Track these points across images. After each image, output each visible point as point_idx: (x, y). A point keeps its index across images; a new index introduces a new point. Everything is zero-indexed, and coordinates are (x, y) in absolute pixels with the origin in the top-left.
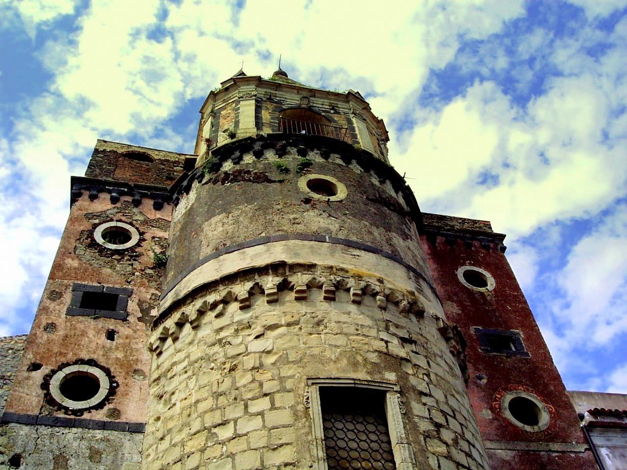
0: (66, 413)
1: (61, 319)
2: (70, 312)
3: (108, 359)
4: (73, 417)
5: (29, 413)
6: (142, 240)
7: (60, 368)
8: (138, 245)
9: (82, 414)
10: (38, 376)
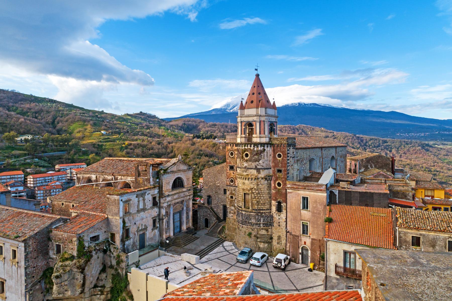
10: (228, 180)
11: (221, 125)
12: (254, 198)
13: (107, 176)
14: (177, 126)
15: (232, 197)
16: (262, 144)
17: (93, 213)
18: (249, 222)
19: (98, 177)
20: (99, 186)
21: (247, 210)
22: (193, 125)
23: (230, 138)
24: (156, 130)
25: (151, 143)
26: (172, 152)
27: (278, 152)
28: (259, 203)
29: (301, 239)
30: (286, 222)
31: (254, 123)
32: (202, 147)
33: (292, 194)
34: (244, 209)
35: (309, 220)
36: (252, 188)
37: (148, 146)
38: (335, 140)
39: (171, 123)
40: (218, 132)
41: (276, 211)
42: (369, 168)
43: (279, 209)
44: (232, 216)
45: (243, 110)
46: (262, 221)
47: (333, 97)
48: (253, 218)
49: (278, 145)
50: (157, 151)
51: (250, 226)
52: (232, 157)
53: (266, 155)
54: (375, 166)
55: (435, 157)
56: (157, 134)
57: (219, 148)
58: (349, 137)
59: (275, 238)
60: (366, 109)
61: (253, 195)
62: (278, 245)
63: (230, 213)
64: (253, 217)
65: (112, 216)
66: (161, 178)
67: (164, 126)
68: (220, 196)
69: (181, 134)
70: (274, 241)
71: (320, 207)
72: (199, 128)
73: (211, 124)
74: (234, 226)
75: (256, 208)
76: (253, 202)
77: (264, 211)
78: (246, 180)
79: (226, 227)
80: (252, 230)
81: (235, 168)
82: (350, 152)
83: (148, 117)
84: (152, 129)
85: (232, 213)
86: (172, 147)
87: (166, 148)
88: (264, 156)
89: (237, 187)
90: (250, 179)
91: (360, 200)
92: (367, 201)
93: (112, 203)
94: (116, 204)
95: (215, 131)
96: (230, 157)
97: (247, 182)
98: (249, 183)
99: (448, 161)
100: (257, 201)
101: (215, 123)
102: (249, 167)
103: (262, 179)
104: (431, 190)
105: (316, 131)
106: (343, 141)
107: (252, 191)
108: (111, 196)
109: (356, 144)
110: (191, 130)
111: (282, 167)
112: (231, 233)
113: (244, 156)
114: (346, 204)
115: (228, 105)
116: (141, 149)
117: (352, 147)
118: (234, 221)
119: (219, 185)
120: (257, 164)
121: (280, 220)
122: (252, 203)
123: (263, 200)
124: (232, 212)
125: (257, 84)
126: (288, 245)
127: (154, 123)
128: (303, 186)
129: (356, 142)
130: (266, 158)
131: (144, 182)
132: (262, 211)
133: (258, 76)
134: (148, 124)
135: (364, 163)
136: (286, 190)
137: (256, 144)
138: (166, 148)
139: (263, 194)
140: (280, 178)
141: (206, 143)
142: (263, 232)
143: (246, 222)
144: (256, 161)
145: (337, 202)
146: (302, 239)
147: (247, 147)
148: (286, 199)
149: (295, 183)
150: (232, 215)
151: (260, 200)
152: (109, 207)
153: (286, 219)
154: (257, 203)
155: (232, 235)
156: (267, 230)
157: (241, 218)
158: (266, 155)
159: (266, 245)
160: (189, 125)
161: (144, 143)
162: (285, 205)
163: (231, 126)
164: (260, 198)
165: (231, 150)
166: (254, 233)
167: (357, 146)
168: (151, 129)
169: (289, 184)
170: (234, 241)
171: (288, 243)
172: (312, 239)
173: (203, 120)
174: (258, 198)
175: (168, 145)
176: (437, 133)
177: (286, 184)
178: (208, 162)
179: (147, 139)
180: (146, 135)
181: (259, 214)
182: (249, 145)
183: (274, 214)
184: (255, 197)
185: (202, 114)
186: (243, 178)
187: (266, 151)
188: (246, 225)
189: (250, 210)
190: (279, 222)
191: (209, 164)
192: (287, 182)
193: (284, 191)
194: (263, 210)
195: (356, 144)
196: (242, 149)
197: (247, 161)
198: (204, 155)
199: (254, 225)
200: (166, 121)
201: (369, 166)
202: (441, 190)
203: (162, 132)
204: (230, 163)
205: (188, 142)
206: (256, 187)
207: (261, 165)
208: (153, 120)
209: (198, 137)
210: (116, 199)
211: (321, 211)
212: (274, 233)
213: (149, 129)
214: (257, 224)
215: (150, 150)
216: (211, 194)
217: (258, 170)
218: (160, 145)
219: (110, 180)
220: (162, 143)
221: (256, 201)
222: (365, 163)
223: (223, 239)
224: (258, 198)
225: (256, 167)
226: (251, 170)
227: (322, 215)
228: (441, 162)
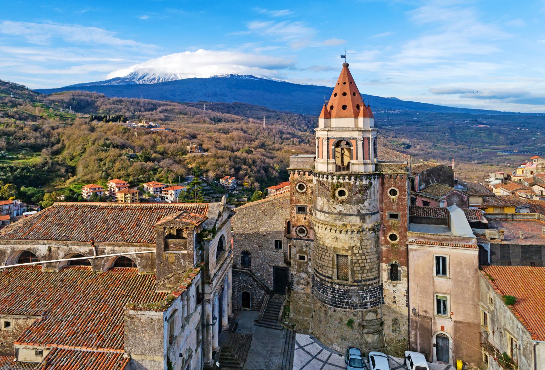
2: (297, 213)
6: (307, 188)
8: (306, 190)
10: (294, 229)
11: (129, 101)
12: (356, 263)
13: (76, 247)
14: (62, 102)
15: (302, 258)
16: (369, 176)
17: (84, 349)
19: (53, 249)
20: (55, 267)
21: (344, 282)
22: (87, 101)
23: (298, 162)
24: (28, 108)
25: (22, 129)
26: (58, 141)
27: (390, 187)
28: (364, 270)
29: (435, 323)
30: (408, 296)
31: (353, 142)
32: (106, 133)
33: (417, 252)
34: (337, 281)
35: (448, 292)
36: (353, 247)
37: (17, 134)
38: (279, 120)
39: (52, 98)
40: (125, 110)
41: (388, 279)
42: (431, 184)
43: (394, 276)
44: (303, 289)
45: (329, 120)
46: (368, 298)
47: (251, 66)
48: (354, 295)
49: (391, 175)
50: (33, 141)
51: (349, 308)
53: (372, 192)
54: (437, 180)
55: (385, 140)
56: (30, 115)
57: (133, 135)
58: (294, 117)
59: (388, 322)
60: (309, 83)
61: (354, 258)
62: (394, 334)
63: (298, 283)
64: (355, 293)
65: (143, 354)
66: (205, 247)
67: (41, 101)
68: (268, 252)
69: (71, 114)
70: (385, 327)
71: (468, 272)
72: (96, 104)
73: (114, 100)
74: (308, 306)
75: (360, 279)
76: (355, 269)
77: (371, 282)
78: (341, 233)
79: (291, 307)
80: (354, 315)
81: (308, 210)
82: (297, 136)
83: (12, 88)
84: (22, 107)
85: (303, 284)
86: (59, 135)
87: (49, 135)
88: (370, 193)
89: (312, 241)
90: (349, 233)
91: (522, 256)
92: (532, 258)
93: (142, 327)
94: (153, 329)
95: (121, 109)
96: (297, 191)
97: (343, 236)
98: (347, 238)
99: (397, 143)
100: (361, 267)
101: (121, 98)
102: (347, 213)
103: (369, 230)
104: (501, 207)
105: (256, 110)
106: (288, 122)
107: (352, 252)
108: (139, 312)
109: (303, 126)
110: (84, 107)
111: (398, 209)
112: (301, 318)
113: (337, 195)
114: (502, 264)
115: (135, 74)
116: (5, 138)
117: (299, 130)
118: (308, 298)
120: (361, 208)
121: (396, 294)
123: (370, 264)
124: (302, 281)
125: (349, 80)
126: (413, 333)
127: (23, 98)
128: (438, 239)
129: (302, 123)
130: (372, 196)
131: (179, 260)
132: (368, 283)
133: (346, 66)
134: (13, 99)
135: (424, 177)
136: (407, 245)
137: (358, 176)
138: (49, 135)
139: (369, 254)
140: (394, 226)
141: (112, 128)
142: (371, 316)
143: (341, 302)
144: (359, 202)
145: (489, 261)
146: (437, 321)
147: (344, 179)
148: (408, 260)
149: (423, 235)
150: (303, 287)
151: (366, 265)
152: (133, 336)
153: (408, 291)
154: (361, 269)
155: (303, 320)
156: (376, 312)
157: (329, 296)
158: (372, 192)
159: (376, 336)
160: (81, 100)
161: (10, 129)
162: (406, 269)
163: (144, 103)
164: (365, 261)
165: (300, 180)
166: (357, 320)
167: (305, 128)
168: (19, 107)
169: (412, 237)
170: (310, 331)
171: (412, 329)
172: (455, 321)
173: (102, 94)
174: (362, 262)
175: (52, 131)
176: (383, 112)
177: (406, 236)
178: (120, 155)
179: (15, 123)
180: (13, 117)
181: (365, 288)
182: (347, 177)
183: (384, 283)
184: (358, 260)
185: (96, 85)
186: (336, 231)
187: (372, 186)
188: (342, 308)
189: (349, 282)
190: (394, 297)
191: (122, 160)
192: (408, 234)
193: (403, 248)
194: (369, 280)
195: (303, 126)
196: (333, 183)
197: (342, 202)
198: (111, 145)
199: (356, 306)
200: (43, 95)
201: (430, 181)
202: (512, 207)
203: (40, 111)
204: (298, 201)
205: (84, 126)
207: (367, 208)
208: (21, 92)
209: (100, 119)
210: (154, 318)
211: (469, 278)
212: (384, 315)
213: (16, 107)
214: (361, 305)
215: (20, 140)
216: (249, 248)
217: (363, 217)
218: (38, 132)
219: (84, 253)
220: (40, 128)
221: (359, 266)
222: (426, 177)
225: (359, 211)
226: (351, 218)
227: (471, 284)
228: (391, 144)
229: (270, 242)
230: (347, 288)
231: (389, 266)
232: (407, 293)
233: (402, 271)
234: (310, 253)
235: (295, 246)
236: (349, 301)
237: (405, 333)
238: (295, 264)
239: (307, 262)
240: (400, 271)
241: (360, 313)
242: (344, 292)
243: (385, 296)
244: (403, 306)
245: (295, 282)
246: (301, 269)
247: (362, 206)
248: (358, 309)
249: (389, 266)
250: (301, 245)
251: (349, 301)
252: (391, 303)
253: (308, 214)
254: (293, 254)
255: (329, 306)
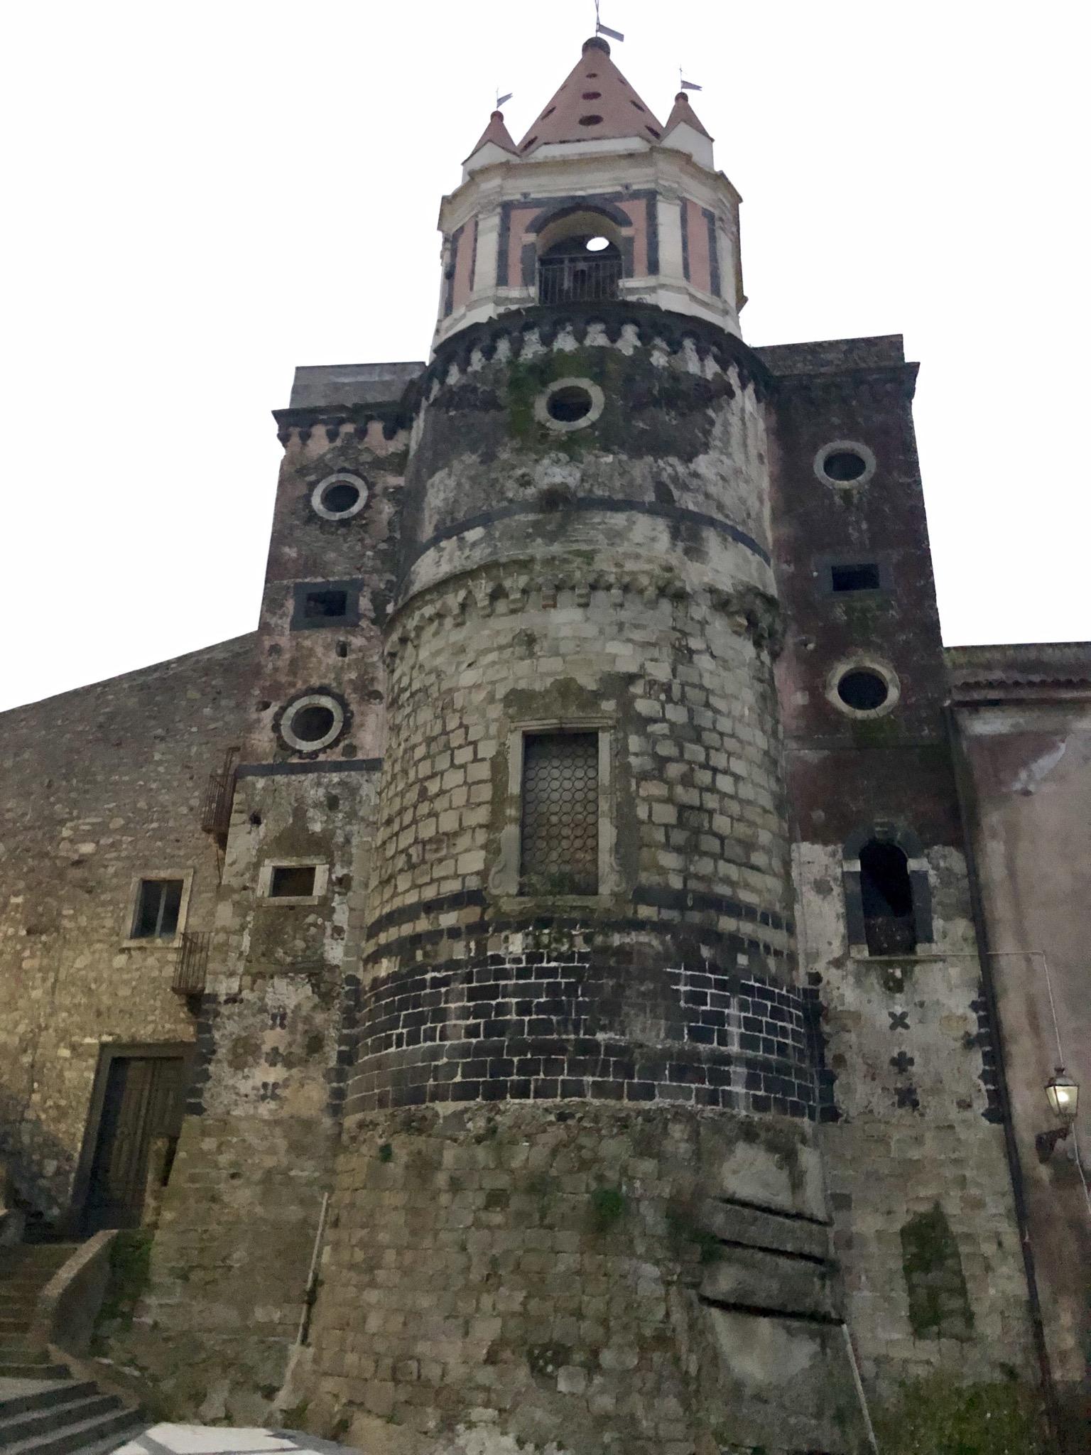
0: (300, 758)
1: (284, 641)
2: (295, 626)
3: (340, 684)
4: (307, 761)
5: (264, 762)
6: (371, 497)
7: (290, 703)
9: (317, 756)
12: (644, 776)
15: (288, 881)
18: (589, 1048)
27: (826, 440)
28: (697, 831)
36: (631, 678)
41: (851, 938)
44: (269, 1092)
46: (734, 1030)
51: (599, 1089)
52: (359, 483)
61: (634, 743)
75: (676, 883)
76: (642, 812)
81: (365, 603)
85: (274, 1057)
100: (682, 808)
107: (626, 704)
112: (224, 1314)
119: (87, 848)
121: (913, 1040)
122: (626, 823)
150: (275, 1074)
154: (681, 823)
164: (704, 777)
181: (705, 952)
183: (831, 976)
184: (662, 761)
190: (902, 1063)
206: (661, 672)
214: (685, 1068)
221: (669, 800)
223: (114, 1403)
224: (687, 781)
229: (106, 897)
230: (588, 939)
231: (847, 856)
232: (982, 1022)
233: (933, 879)
234: (348, 841)
235: (256, 820)
236: (600, 1036)
237: (1006, 1330)
238: (243, 928)
239: (325, 901)
240: (923, 876)
241: (678, 1131)
242: (566, 972)
243: (840, 1060)
244: (968, 1114)
245: (222, 1052)
246: (280, 953)
247: (681, 469)
248: (666, 1092)
249: (847, 856)
250: (300, 800)
251: (600, 1036)
252: (883, 1105)
253: (364, 623)
254: (240, 866)
255: (445, 1108)
